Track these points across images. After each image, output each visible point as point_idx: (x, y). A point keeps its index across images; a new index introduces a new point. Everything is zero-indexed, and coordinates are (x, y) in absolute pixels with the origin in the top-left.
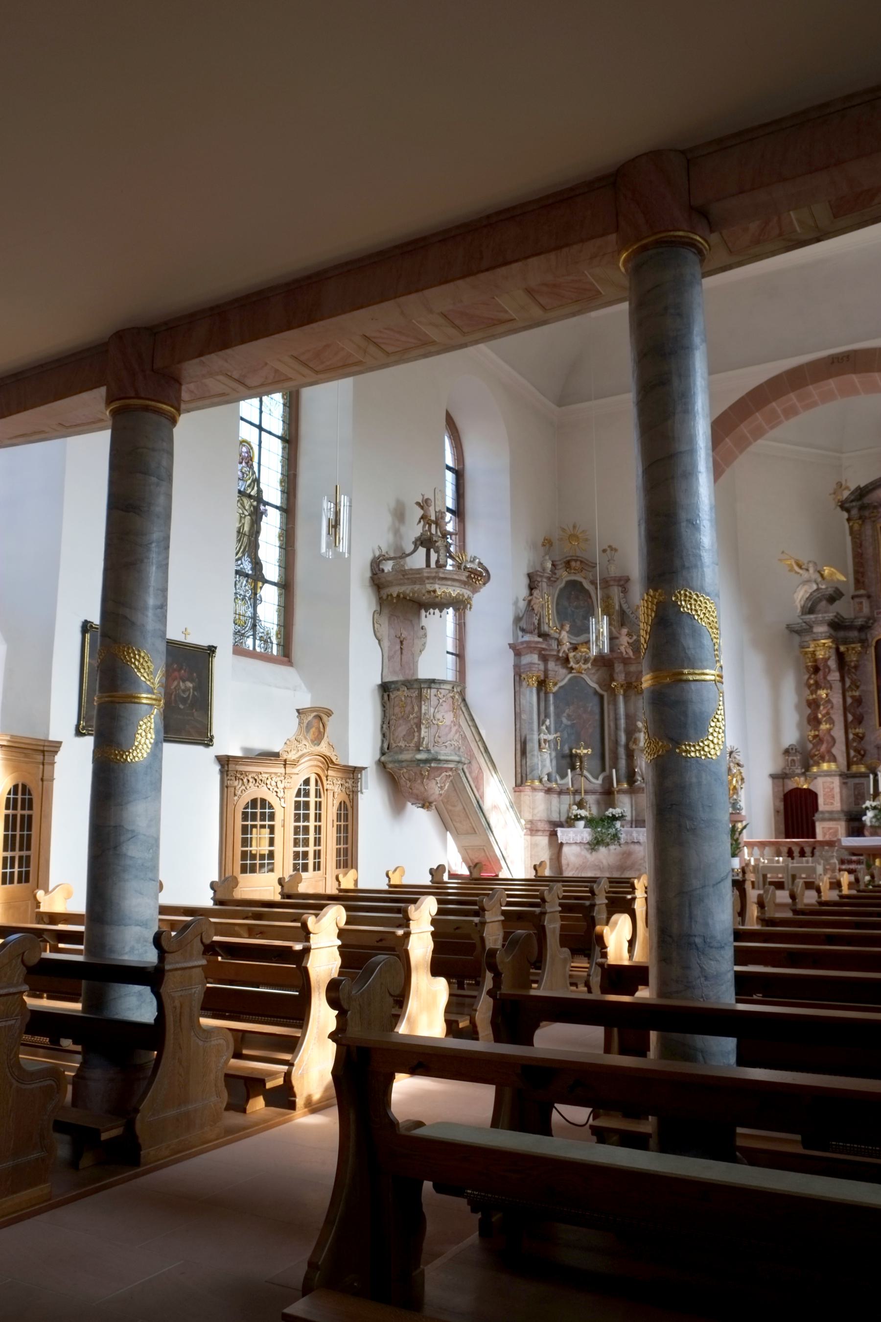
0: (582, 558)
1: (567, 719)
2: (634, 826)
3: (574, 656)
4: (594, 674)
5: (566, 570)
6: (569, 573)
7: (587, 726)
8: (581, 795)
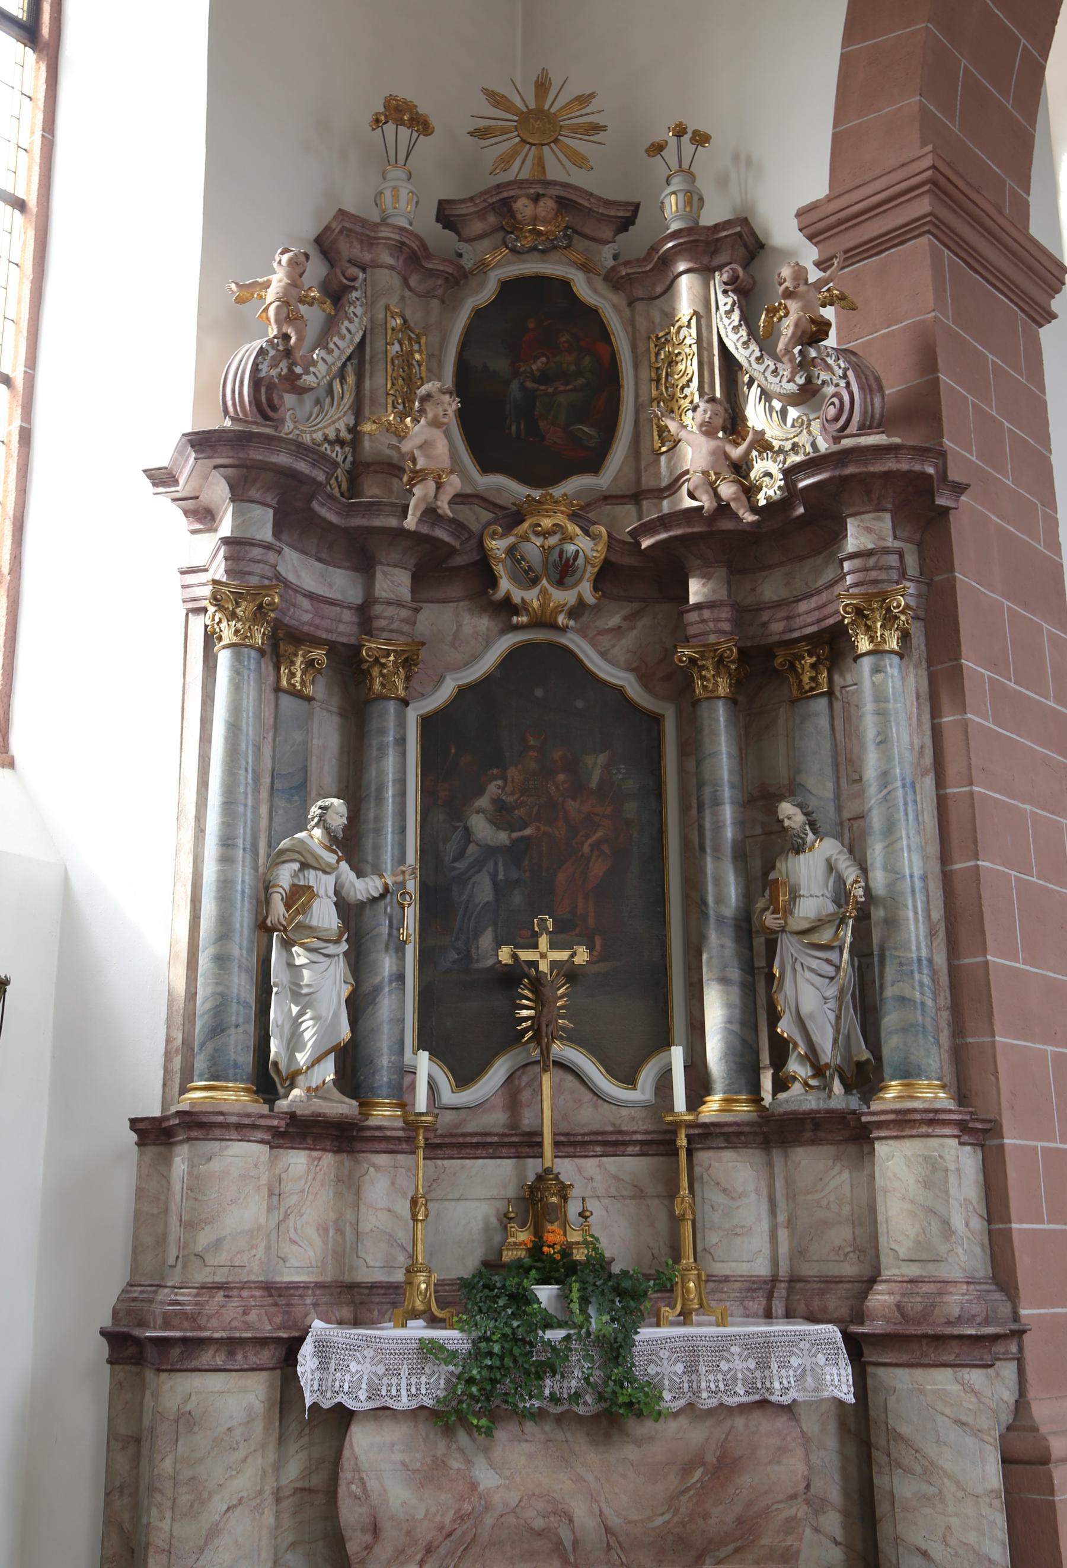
0: (566, 186)
1: (491, 822)
2: (778, 1307)
3: (511, 550)
6: (514, 250)
7: (586, 849)
8: (541, 1156)
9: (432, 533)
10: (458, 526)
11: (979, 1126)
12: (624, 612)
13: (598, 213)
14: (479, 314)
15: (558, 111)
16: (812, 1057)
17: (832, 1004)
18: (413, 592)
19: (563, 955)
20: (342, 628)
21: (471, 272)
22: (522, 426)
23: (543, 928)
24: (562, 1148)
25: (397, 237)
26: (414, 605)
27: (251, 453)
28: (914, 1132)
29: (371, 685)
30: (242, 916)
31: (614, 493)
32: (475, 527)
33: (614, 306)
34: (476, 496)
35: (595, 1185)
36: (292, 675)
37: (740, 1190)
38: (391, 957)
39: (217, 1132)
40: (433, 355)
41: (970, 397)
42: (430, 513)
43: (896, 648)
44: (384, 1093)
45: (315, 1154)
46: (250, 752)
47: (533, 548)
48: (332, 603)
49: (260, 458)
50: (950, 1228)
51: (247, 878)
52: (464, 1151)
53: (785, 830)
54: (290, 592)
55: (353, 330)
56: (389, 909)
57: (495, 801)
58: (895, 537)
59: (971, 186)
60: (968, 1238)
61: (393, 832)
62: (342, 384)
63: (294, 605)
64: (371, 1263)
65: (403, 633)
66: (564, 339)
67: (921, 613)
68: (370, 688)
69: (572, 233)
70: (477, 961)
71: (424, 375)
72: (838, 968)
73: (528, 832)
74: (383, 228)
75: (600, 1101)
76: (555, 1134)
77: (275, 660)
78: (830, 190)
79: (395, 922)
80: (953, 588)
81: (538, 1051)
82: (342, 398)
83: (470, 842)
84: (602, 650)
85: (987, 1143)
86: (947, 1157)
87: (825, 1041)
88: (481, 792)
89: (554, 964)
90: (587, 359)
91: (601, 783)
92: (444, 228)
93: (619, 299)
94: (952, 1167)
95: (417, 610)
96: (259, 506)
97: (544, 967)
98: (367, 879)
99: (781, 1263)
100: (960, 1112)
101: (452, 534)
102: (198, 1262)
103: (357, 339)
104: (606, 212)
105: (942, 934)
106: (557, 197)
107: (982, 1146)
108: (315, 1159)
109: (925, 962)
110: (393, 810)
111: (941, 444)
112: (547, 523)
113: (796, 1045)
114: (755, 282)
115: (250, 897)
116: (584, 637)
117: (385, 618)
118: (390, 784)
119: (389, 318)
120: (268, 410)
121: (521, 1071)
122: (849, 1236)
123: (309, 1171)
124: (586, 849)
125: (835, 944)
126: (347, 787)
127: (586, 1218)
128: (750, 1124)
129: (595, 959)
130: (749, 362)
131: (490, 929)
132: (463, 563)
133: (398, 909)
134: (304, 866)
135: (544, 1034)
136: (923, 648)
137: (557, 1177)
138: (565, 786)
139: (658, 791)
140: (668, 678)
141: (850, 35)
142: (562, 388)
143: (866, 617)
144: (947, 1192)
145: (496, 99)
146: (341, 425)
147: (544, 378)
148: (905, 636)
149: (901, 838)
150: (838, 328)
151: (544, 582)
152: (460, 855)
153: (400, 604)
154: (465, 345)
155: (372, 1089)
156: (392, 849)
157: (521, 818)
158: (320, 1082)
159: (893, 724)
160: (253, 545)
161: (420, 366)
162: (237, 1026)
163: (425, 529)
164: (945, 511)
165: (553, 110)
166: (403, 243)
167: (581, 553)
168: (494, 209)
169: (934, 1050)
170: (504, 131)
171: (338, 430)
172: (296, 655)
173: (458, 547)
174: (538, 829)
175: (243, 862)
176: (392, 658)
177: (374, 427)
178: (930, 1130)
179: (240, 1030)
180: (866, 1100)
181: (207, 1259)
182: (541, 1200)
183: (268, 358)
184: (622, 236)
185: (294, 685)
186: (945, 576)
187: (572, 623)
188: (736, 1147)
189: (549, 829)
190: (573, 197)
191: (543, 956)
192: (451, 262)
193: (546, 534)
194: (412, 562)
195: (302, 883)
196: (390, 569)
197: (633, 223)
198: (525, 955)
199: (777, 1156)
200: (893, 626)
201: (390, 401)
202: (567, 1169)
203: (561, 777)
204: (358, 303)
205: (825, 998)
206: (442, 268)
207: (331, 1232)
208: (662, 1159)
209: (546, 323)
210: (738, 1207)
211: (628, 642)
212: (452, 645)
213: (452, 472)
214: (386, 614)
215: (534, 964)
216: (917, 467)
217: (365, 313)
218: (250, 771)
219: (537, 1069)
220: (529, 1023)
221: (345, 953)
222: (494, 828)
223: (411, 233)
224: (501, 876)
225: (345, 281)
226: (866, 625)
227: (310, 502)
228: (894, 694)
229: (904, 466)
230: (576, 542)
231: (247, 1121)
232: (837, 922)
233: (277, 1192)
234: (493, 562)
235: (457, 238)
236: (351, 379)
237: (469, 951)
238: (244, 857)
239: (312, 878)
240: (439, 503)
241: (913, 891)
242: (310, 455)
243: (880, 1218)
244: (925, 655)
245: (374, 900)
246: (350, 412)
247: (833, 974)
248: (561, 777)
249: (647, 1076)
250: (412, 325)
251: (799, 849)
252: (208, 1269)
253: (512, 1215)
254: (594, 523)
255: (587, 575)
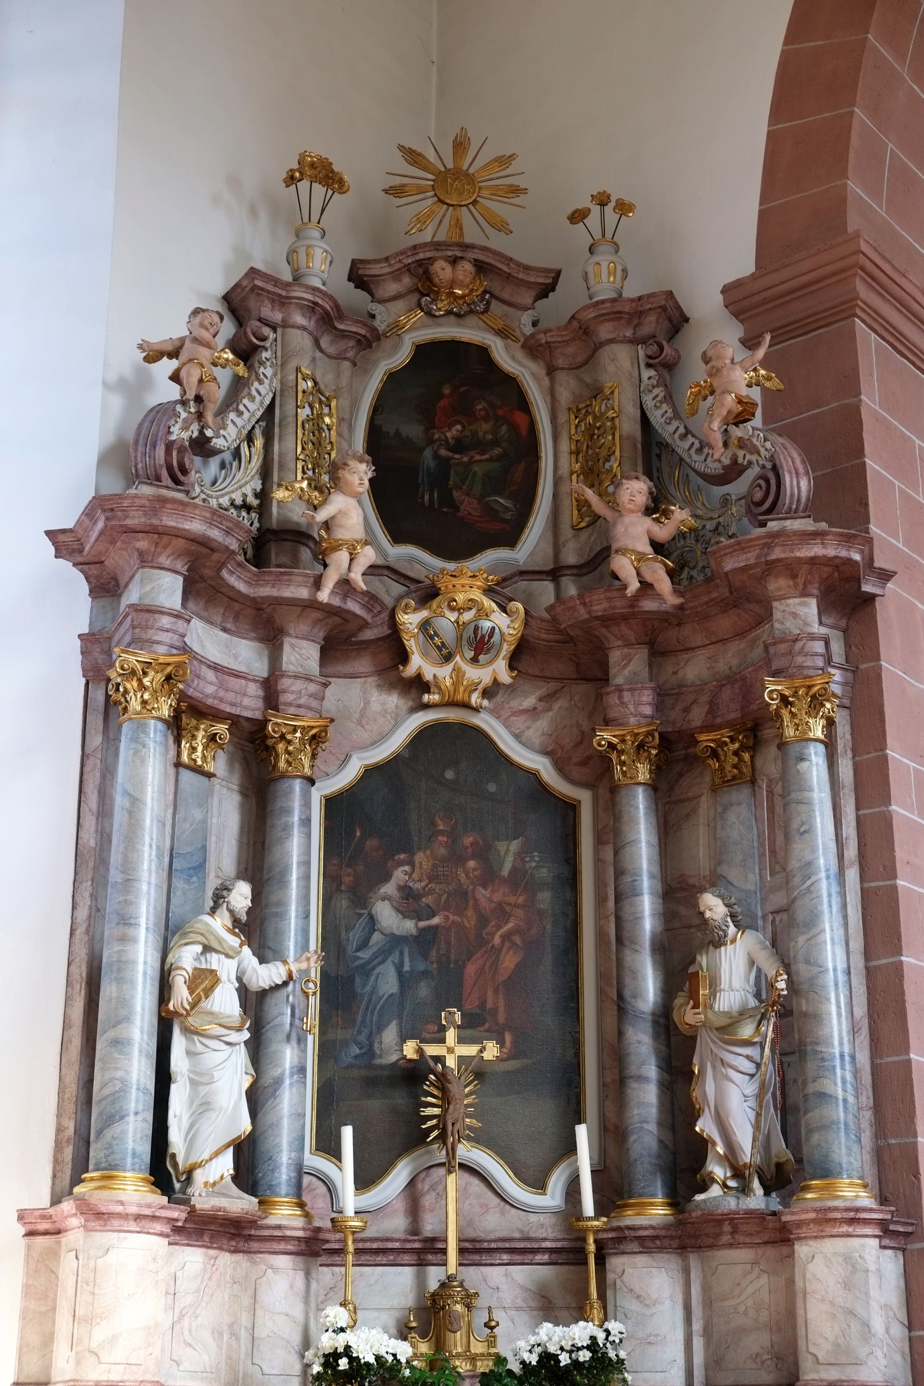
0: (484, 249)
1: (398, 910)
3: (425, 625)
4: (533, 712)
5: (419, 306)
6: (429, 314)
7: (497, 940)
8: (445, 1264)
9: (343, 606)
10: (371, 599)
11: (900, 1229)
12: (539, 693)
13: (518, 278)
14: (393, 378)
15: (476, 172)
16: (731, 1159)
17: (752, 1103)
18: (321, 666)
19: (470, 1050)
20: (246, 701)
21: (384, 334)
22: (436, 496)
23: (452, 1023)
24: (467, 1254)
25: (310, 297)
26: (323, 680)
27: (164, 518)
28: (835, 1231)
29: (276, 762)
30: (143, 998)
31: (531, 569)
32: (389, 601)
33: (533, 375)
34: (388, 568)
35: (501, 1295)
36: (193, 749)
37: (655, 1296)
38: (293, 1049)
39: (116, 1223)
40: (343, 419)
41: (897, 483)
42: (345, 584)
43: (822, 737)
44: (283, 1192)
45: (212, 1252)
46: (155, 828)
47: (447, 622)
48: (237, 675)
49: (173, 524)
50: (870, 1331)
51: (149, 959)
52: (363, 1258)
53: (705, 922)
54: (195, 663)
55: (263, 392)
56: (291, 998)
57: (403, 889)
58: (821, 623)
59: (898, 270)
60: (888, 1345)
61: (297, 917)
62: (249, 447)
63: (199, 677)
64: (266, 1370)
65: (310, 709)
66: (479, 407)
67: (847, 702)
68: (275, 766)
69: (488, 296)
70: (381, 1056)
71: (333, 439)
72: (758, 1066)
73: (436, 921)
74: (296, 288)
75: (508, 1207)
76: (460, 1240)
77: (175, 733)
78: (756, 269)
79: (297, 1011)
80: (879, 677)
81: (444, 1152)
82: (250, 462)
83: (374, 930)
84: (517, 731)
85: (909, 1247)
86: (867, 1257)
87: (745, 1138)
88: (387, 877)
89: (461, 1060)
90: (504, 428)
91: (514, 870)
92: (356, 287)
93: (538, 368)
94: (872, 1268)
95: (326, 685)
96: (169, 573)
97: (451, 1062)
98: (270, 965)
99: (696, 1373)
100: (881, 1211)
101: (364, 606)
102: (93, 1359)
103: (267, 401)
104: (525, 278)
105: (865, 1031)
106: (475, 260)
107: (904, 1250)
108: (211, 1258)
109: (847, 1058)
110: (297, 894)
111: (867, 531)
112: (460, 598)
113: (714, 1144)
114: (679, 357)
115: (152, 978)
116: (498, 717)
117: (292, 692)
118: (295, 866)
119: (300, 380)
120: (179, 474)
121: (424, 1174)
122: (767, 1344)
123: (205, 1270)
124: (497, 940)
125: (756, 1040)
126: (246, 869)
127: (492, 1328)
128: (667, 1227)
129: (506, 1056)
130: (674, 440)
131: (394, 1022)
132: (373, 637)
133: (302, 998)
134: (207, 949)
135: (449, 1133)
136: (848, 737)
137: (461, 1285)
138: (476, 873)
139: (572, 881)
140: (584, 763)
141: (777, 112)
142: (478, 457)
143: (791, 704)
144: (867, 1294)
145: (413, 157)
146: (248, 490)
147: (459, 446)
148: (830, 723)
149: (824, 930)
150: (763, 408)
151: (458, 658)
152: (364, 944)
153: (308, 679)
154: (376, 410)
155: (271, 1187)
156: (296, 935)
157: (428, 906)
158: (217, 1177)
159: (817, 813)
160: (162, 613)
161: (329, 430)
162: (136, 1113)
163: (336, 602)
164: (871, 599)
165: (471, 171)
166: (316, 304)
167: (497, 630)
168: (409, 270)
169: (855, 1148)
170: (421, 190)
171: (245, 495)
172: (197, 729)
173: (369, 620)
174: (447, 918)
175: (146, 942)
176: (298, 735)
177: (287, 493)
178: (851, 1230)
179: (140, 1118)
180: (785, 1203)
181: (101, 1356)
182: (443, 1308)
183: (180, 421)
184: (540, 303)
185: (195, 761)
186: (872, 664)
187: (485, 703)
188: (651, 1252)
189: (457, 919)
190: (492, 261)
191: (451, 1050)
192: (364, 324)
193: (460, 610)
194: (321, 635)
195: (204, 966)
196: (299, 641)
197: (553, 290)
198: (432, 1050)
199: (694, 1262)
200: (818, 713)
201: (299, 466)
202: (473, 1276)
203: (472, 864)
204: (268, 364)
205: (745, 1096)
206: (354, 329)
207: (226, 1337)
208: (571, 1268)
209: (462, 389)
210: (652, 1315)
211: (543, 724)
212: (359, 722)
213: (366, 543)
214: (294, 688)
215: (439, 1059)
216: (843, 553)
217: (275, 374)
218: (154, 847)
219: (442, 1171)
220: (434, 1122)
221: (246, 1043)
222: (400, 916)
223: (324, 294)
224: (407, 967)
225: (255, 341)
226: (791, 712)
227: (219, 570)
228: (818, 784)
229: (831, 552)
230: (492, 617)
231: (147, 1212)
232: (759, 1017)
233: (172, 1291)
234: (405, 636)
235: (370, 298)
236: (259, 442)
237: (371, 1046)
238: (146, 937)
239: (215, 961)
240: (352, 575)
241: (836, 984)
242: (224, 522)
243: (800, 1321)
244: (850, 744)
245: (277, 987)
246: (257, 476)
247: (753, 1071)
248: (472, 864)
249: (557, 1181)
250: (322, 387)
251: (719, 943)
252: (103, 1367)
253: (414, 1324)
254: (511, 600)
255: (503, 653)
